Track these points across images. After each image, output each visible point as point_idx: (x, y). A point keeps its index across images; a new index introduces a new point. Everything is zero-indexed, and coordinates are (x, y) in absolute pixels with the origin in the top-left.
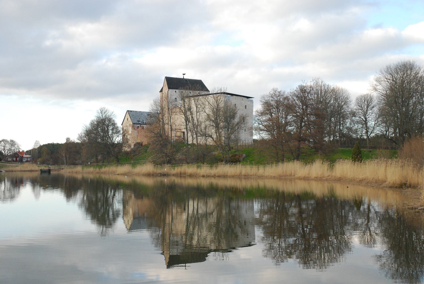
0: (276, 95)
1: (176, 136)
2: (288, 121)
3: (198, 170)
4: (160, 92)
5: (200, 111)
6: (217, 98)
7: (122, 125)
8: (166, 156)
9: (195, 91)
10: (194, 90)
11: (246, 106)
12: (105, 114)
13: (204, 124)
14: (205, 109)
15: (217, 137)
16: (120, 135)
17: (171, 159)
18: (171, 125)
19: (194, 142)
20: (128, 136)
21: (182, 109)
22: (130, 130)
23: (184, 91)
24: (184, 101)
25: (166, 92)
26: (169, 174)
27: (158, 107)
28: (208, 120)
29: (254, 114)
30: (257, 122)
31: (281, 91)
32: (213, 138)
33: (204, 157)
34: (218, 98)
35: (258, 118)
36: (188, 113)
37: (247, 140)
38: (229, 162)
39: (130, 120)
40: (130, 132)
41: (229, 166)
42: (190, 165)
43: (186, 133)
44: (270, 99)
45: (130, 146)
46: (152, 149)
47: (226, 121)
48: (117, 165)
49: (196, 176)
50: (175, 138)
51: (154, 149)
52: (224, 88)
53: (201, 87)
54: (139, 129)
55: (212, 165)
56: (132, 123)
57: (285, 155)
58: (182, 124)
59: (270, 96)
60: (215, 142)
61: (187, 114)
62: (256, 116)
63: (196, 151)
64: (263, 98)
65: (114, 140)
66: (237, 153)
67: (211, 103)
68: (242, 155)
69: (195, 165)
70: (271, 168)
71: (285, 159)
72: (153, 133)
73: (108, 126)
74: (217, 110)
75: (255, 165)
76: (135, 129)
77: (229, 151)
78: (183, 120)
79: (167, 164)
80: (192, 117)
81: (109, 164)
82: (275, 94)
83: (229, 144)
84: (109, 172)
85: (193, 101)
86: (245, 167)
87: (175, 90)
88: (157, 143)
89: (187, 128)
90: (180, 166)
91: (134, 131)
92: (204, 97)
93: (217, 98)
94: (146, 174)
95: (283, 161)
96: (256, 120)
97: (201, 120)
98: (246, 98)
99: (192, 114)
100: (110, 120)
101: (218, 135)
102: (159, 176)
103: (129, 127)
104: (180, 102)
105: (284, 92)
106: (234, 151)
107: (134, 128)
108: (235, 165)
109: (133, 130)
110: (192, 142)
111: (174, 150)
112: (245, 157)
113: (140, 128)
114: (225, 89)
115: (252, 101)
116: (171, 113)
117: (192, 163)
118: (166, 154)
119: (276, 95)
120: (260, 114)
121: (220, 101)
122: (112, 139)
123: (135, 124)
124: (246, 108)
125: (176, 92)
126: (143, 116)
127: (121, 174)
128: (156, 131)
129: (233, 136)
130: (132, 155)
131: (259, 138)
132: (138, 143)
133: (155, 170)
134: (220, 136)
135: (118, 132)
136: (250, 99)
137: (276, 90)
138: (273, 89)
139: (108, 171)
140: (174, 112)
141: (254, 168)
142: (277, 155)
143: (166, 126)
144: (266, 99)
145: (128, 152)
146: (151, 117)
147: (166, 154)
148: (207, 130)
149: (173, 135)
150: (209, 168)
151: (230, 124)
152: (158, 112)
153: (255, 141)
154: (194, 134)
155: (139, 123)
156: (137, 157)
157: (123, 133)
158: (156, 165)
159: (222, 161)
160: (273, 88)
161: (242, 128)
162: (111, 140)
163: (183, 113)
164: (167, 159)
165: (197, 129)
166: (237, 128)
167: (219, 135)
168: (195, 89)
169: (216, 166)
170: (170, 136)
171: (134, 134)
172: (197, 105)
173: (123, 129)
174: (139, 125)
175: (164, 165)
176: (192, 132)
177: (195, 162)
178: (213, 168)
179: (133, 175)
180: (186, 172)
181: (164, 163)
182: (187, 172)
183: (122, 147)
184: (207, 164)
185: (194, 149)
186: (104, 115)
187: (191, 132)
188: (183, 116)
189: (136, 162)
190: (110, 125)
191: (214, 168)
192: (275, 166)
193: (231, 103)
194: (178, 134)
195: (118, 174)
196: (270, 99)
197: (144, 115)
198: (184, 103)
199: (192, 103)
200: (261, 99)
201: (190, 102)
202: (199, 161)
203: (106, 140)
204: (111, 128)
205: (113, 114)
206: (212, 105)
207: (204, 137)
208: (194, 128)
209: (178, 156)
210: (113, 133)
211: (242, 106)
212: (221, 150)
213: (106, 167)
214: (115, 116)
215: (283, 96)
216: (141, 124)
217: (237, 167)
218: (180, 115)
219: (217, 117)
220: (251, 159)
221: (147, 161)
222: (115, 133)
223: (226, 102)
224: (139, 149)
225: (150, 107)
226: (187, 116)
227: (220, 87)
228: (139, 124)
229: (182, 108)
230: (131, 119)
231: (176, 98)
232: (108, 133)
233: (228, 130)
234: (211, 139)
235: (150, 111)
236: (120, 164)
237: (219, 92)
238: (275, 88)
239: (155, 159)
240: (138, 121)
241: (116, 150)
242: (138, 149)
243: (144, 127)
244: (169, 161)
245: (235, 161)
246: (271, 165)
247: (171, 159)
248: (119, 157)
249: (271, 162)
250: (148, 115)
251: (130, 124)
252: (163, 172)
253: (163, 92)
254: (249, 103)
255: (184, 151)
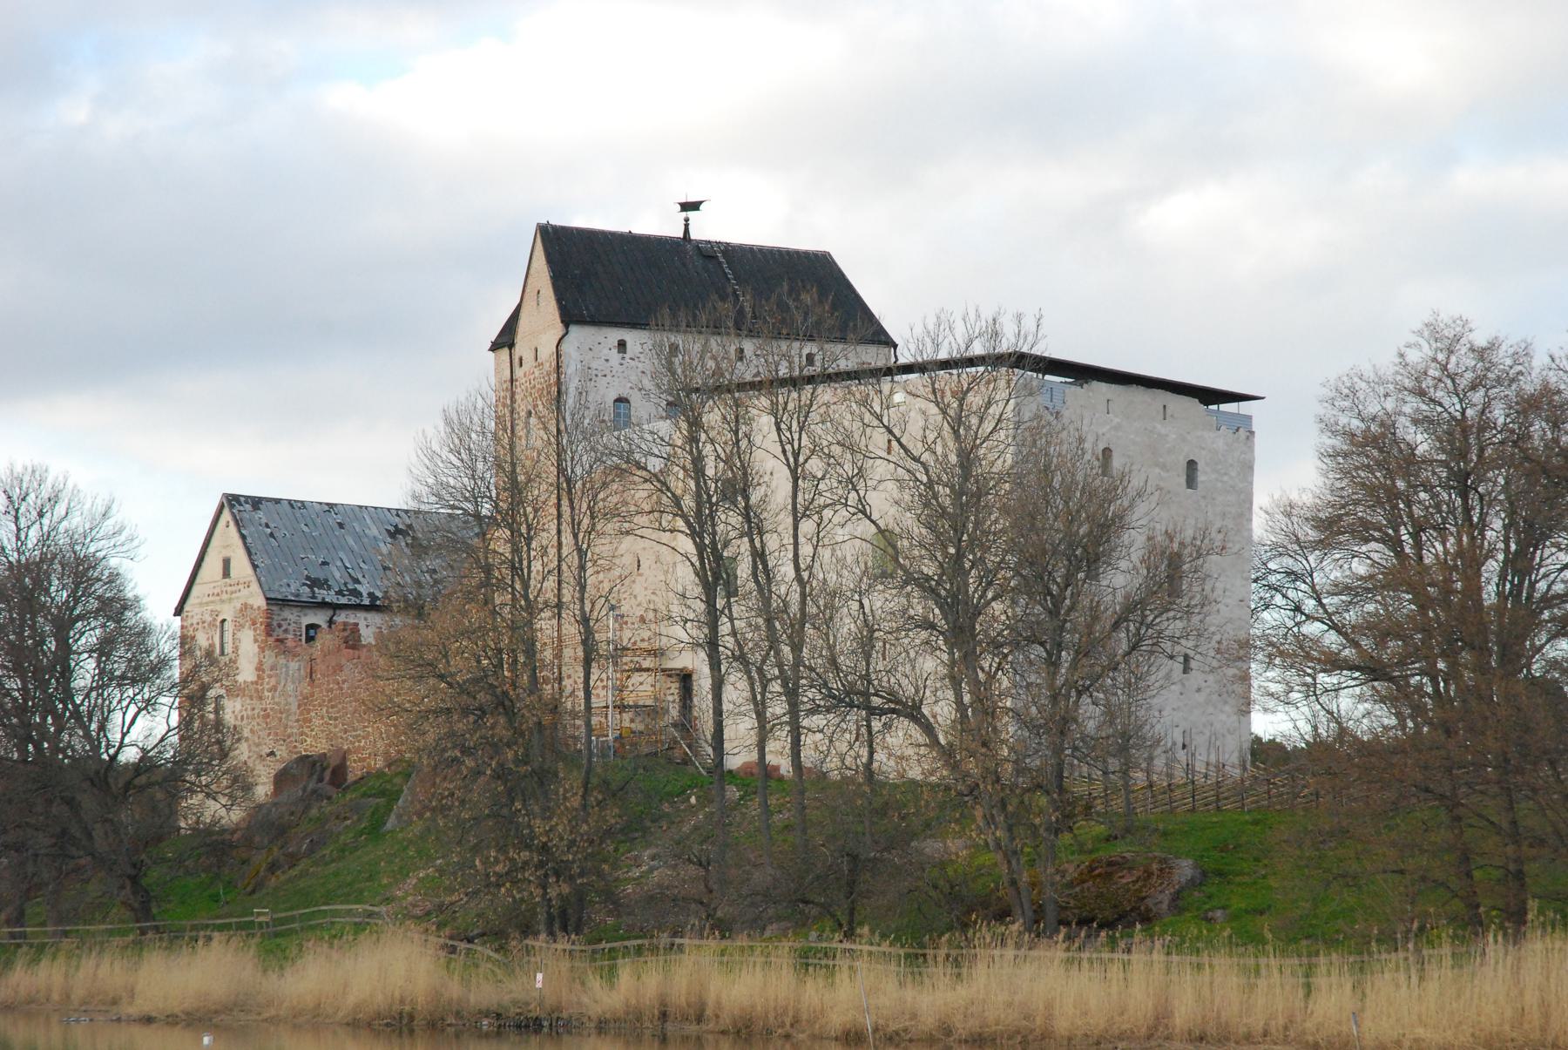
0: (1452, 377)
1: (622, 708)
2: (1542, 586)
3: (810, 983)
4: (495, 347)
5: (821, 501)
6: (961, 402)
7: (179, 611)
8: (541, 865)
9: (784, 345)
10: (778, 336)
11: (1192, 465)
12: (46, 521)
13: (855, 606)
14: (861, 486)
15: (964, 716)
16: (162, 700)
17: (580, 897)
18: (585, 620)
19: (771, 759)
20: (226, 702)
21: (677, 486)
22: (247, 652)
23: (691, 344)
24: (695, 424)
25: (547, 351)
26: (565, 1015)
27: (480, 465)
28: (884, 575)
29: (1259, 527)
30: (1279, 600)
31: (1493, 346)
32: (928, 729)
33: (852, 884)
34: (970, 397)
35: (1288, 562)
36: (729, 521)
37: (1200, 741)
38: (1067, 924)
39: (249, 570)
40: (246, 674)
41: (1059, 953)
42: (742, 941)
43: (703, 683)
44: (1407, 409)
45: (241, 783)
46: (433, 810)
47: (1034, 579)
48: (139, 946)
49: (787, 1037)
50: (612, 725)
51: (443, 810)
52: (1019, 318)
53: (834, 307)
54: (318, 644)
55: (923, 946)
56: (259, 602)
57: (1531, 868)
58: (676, 609)
59: (1408, 383)
60: (947, 753)
61: (720, 528)
62: (1279, 551)
63: (788, 828)
64: (1347, 404)
65: (115, 736)
66: (1121, 849)
67: (912, 434)
68: (1166, 870)
69: (786, 945)
70: (1414, 979)
71: (1533, 905)
72: (442, 677)
73: (64, 625)
74: (957, 494)
75: (1284, 953)
76: (290, 643)
77: (1057, 832)
78: (686, 577)
79: (551, 933)
80: (759, 555)
81: (66, 934)
82: (1444, 368)
83: (1060, 777)
84: (67, 997)
85: (765, 422)
86: (1199, 967)
87: (614, 335)
88: (469, 762)
89: (712, 645)
90: (654, 950)
91: (282, 660)
92: (858, 389)
93: (961, 402)
94: (379, 1015)
95: (1515, 921)
96: (1273, 579)
97: (832, 578)
98: (1192, 405)
99: (753, 525)
100: (82, 570)
101: (967, 699)
102: (487, 1036)
103: (239, 627)
104: (664, 427)
105: (1523, 354)
106: (1101, 829)
107: (281, 641)
108: (1112, 944)
109: (270, 657)
110: (754, 756)
111: (612, 816)
112: (1193, 884)
113: (325, 640)
114: (1029, 324)
115: (1243, 427)
116: (586, 522)
117: (757, 925)
118: (544, 848)
119: (1452, 377)
120: (1308, 533)
121: (988, 426)
122: (94, 726)
123: (284, 603)
124: (1191, 481)
125: (622, 345)
126: (351, 541)
127: (172, 1020)
128: (461, 667)
129: (1090, 715)
130: (260, 859)
131: (1306, 728)
132: (310, 765)
133: (454, 990)
134: (986, 707)
135: (143, 673)
136: (1225, 407)
137: (1457, 339)
138: (1433, 331)
139: (55, 997)
140: (613, 513)
141: (1275, 972)
142: (1469, 875)
143: (545, 625)
144: (1373, 408)
145: (223, 831)
146: (419, 550)
147: (544, 848)
148: (878, 664)
149: (601, 697)
150: (893, 967)
151: (1071, 609)
152: (486, 509)
153: (1265, 752)
154: (776, 687)
155: (322, 594)
156: (1482, 450)
157: (185, 681)
158: (463, 945)
159: (1003, 915)
160: (1427, 318)
161: (1167, 645)
162: (86, 729)
163: (685, 517)
164: (552, 893)
165: (797, 648)
166: (1124, 646)
167: (978, 699)
168: (785, 330)
169: (954, 953)
170: (573, 701)
171: (274, 689)
172: (796, 455)
173: (186, 641)
174: (319, 618)
175: (529, 942)
176: (760, 671)
177: (779, 918)
178: (932, 970)
179: (272, 1020)
180: (711, 1003)
181: (527, 930)
182: (718, 1003)
183: (174, 797)
184: (884, 936)
185: (767, 811)
186: (34, 534)
187: (748, 673)
188: (687, 545)
189: (292, 919)
190: (80, 617)
191: (939, 973)
192: (1448, 962)
193: (1081, 440)
194: (643, 688)
195: (148, 1020)
196: (1407, 409)
197: (358, 537)
198: (693, 439)
199: (758, 440)
200: (1329, 412)
201: (743, 428)
202: (815, 911)
203: (44, 735)
204: (88, 636)
205: (108, 526)
206: (915, 459)
207: (853, 716)
208: (774, 643)
209: (636, 873)
210: (105, 678)
211: (1164, 467)
212: (990, 820)
213: (45, 962)
214: (122, 538)
215: (1513, 380)
216: (336, 607)
217: (1126, 965)
218: (656, 535)
219: (960, 556)
220: (1238, 904)
221: (383, 909)
222: (123, 677)
223: (1035, 432)
224: (314, 812)
225: (420, 470)
226: (714, 542)
227: (987, 314)
228: (324, 605)
229: (681, 483)
230: (255, 567)
231: (620, 400)
232: (67, 674)
233: (1053, 663)
234: (917, 734)
235: (416, 497)
236: (157, 929)
237: (978, 349)
238: (1445, 317)
239: (451, 890)
240: (314, 583)
241: (129, 816)
242: (308, 808)
243: (363, 631)
244: (563, 913)
245: (1109, 914)
246: (1418, 950)
247: (580, 897)
248: (153, 876)
249: (1416, 925)
250: (395, 533)
251: (245, 607)
252: (515, 1003)
253: (522, 348)
254: (1219, 441)
255: (686, 829)
